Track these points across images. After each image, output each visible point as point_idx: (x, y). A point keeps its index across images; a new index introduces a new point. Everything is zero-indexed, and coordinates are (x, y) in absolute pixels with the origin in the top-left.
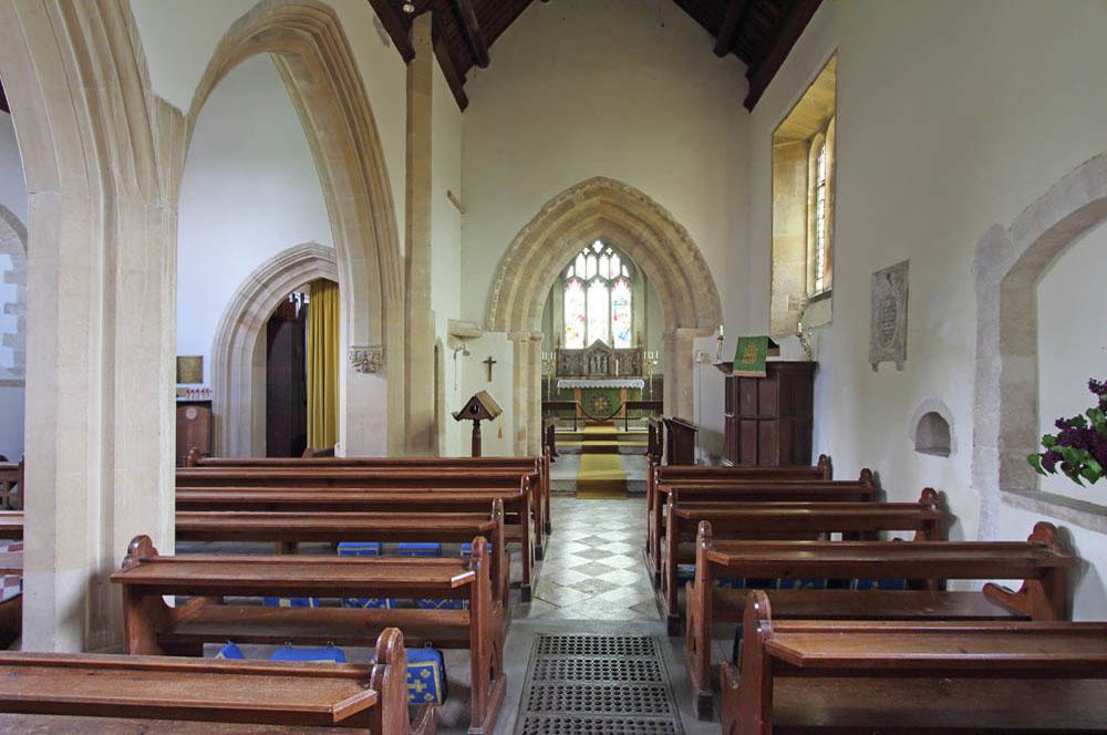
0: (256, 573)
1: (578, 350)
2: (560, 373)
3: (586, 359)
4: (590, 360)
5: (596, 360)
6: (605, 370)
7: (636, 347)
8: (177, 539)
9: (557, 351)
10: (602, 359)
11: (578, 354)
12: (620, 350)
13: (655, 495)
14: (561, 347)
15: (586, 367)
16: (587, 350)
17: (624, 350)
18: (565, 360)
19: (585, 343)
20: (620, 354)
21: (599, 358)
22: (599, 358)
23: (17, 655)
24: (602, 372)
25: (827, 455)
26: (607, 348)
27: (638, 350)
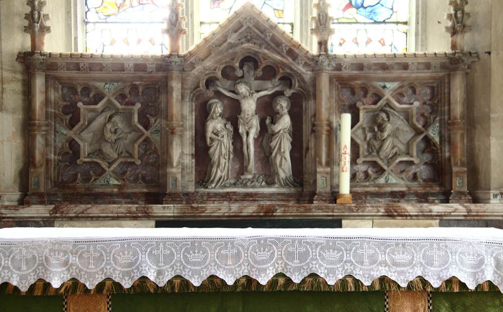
0: (255, 154)
1: (140, 66)
2: (40, 179)
3: (182, 111)
4: (203, 114)
5: (234, 115)
6: (284, 167)
7: (440, 44)
8: (54, 227)
9: (29, 62)
10: (267, 110)
11: (145, 88)
12: (360, 65)
13: (339, 218)
14: (53, 44)
15: (181, 153)
16: (186, 63)
17: (385, 65)
18: (73, 117)
19: (175, 28)
20: (358, 84)
21: (249, 106)
22: (249, 106)
23: (329, 109)
24: (270, 177)
25: (27, 2)
26: (293, 52)
27: (453, 63)
